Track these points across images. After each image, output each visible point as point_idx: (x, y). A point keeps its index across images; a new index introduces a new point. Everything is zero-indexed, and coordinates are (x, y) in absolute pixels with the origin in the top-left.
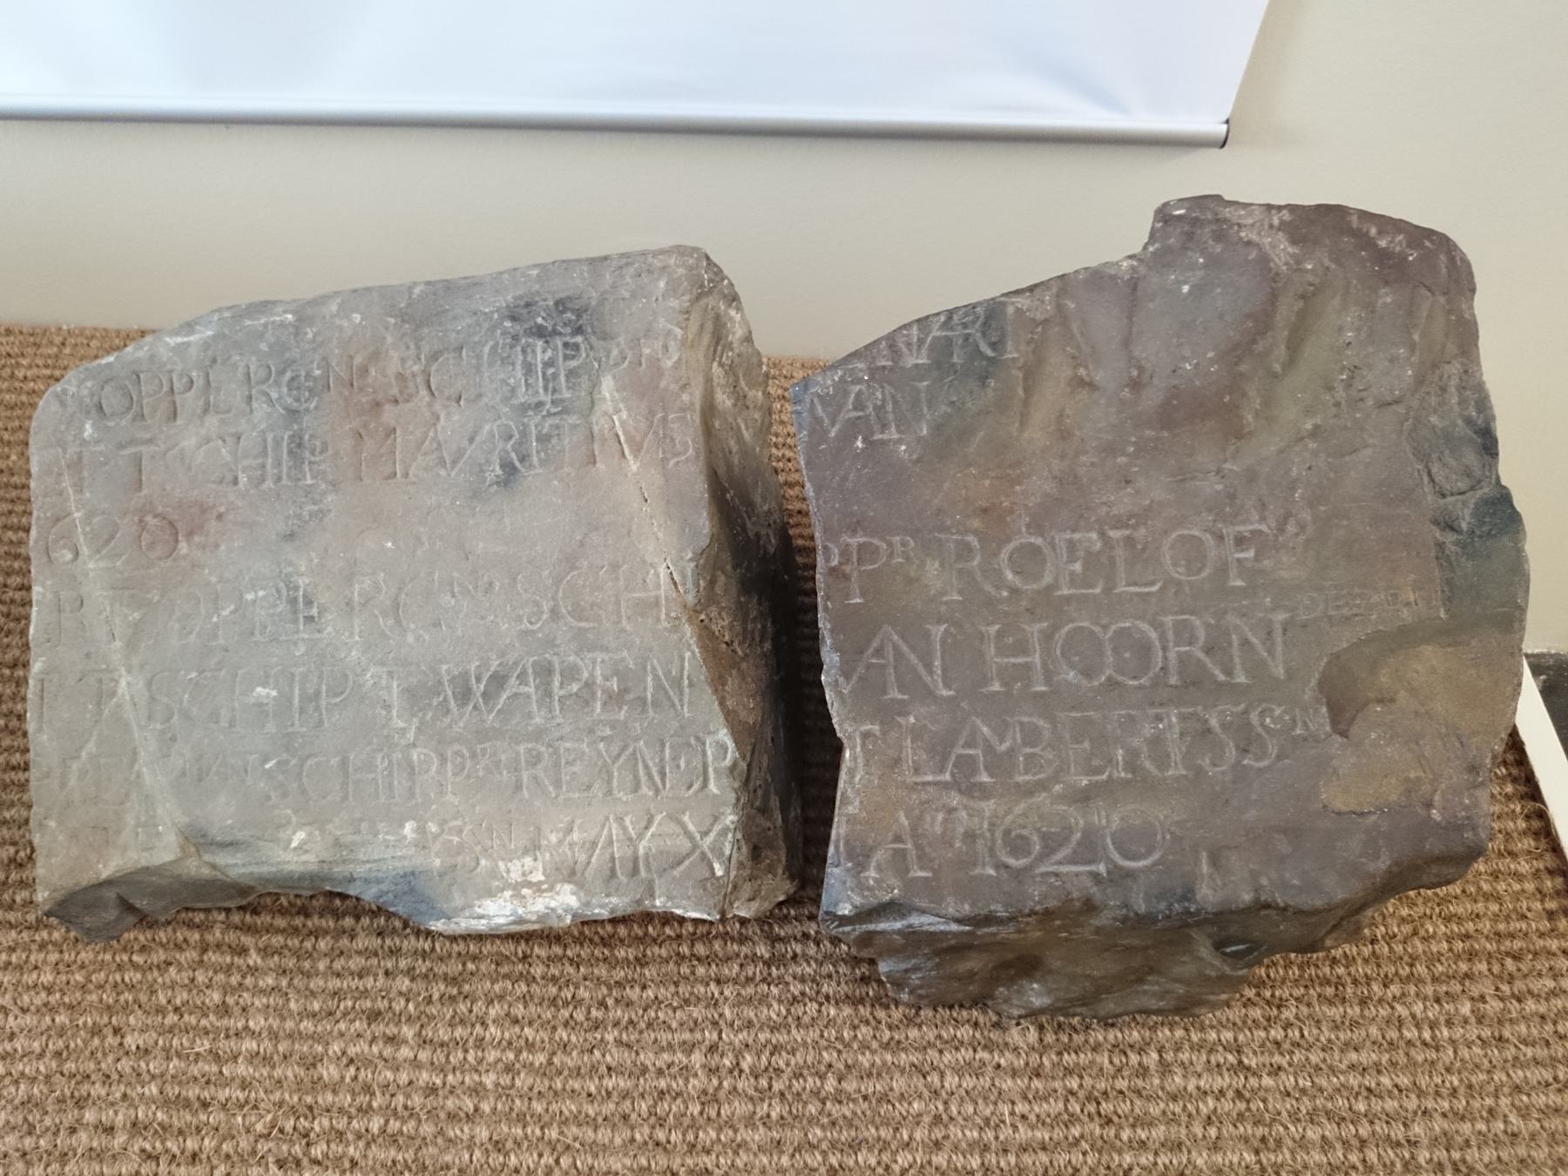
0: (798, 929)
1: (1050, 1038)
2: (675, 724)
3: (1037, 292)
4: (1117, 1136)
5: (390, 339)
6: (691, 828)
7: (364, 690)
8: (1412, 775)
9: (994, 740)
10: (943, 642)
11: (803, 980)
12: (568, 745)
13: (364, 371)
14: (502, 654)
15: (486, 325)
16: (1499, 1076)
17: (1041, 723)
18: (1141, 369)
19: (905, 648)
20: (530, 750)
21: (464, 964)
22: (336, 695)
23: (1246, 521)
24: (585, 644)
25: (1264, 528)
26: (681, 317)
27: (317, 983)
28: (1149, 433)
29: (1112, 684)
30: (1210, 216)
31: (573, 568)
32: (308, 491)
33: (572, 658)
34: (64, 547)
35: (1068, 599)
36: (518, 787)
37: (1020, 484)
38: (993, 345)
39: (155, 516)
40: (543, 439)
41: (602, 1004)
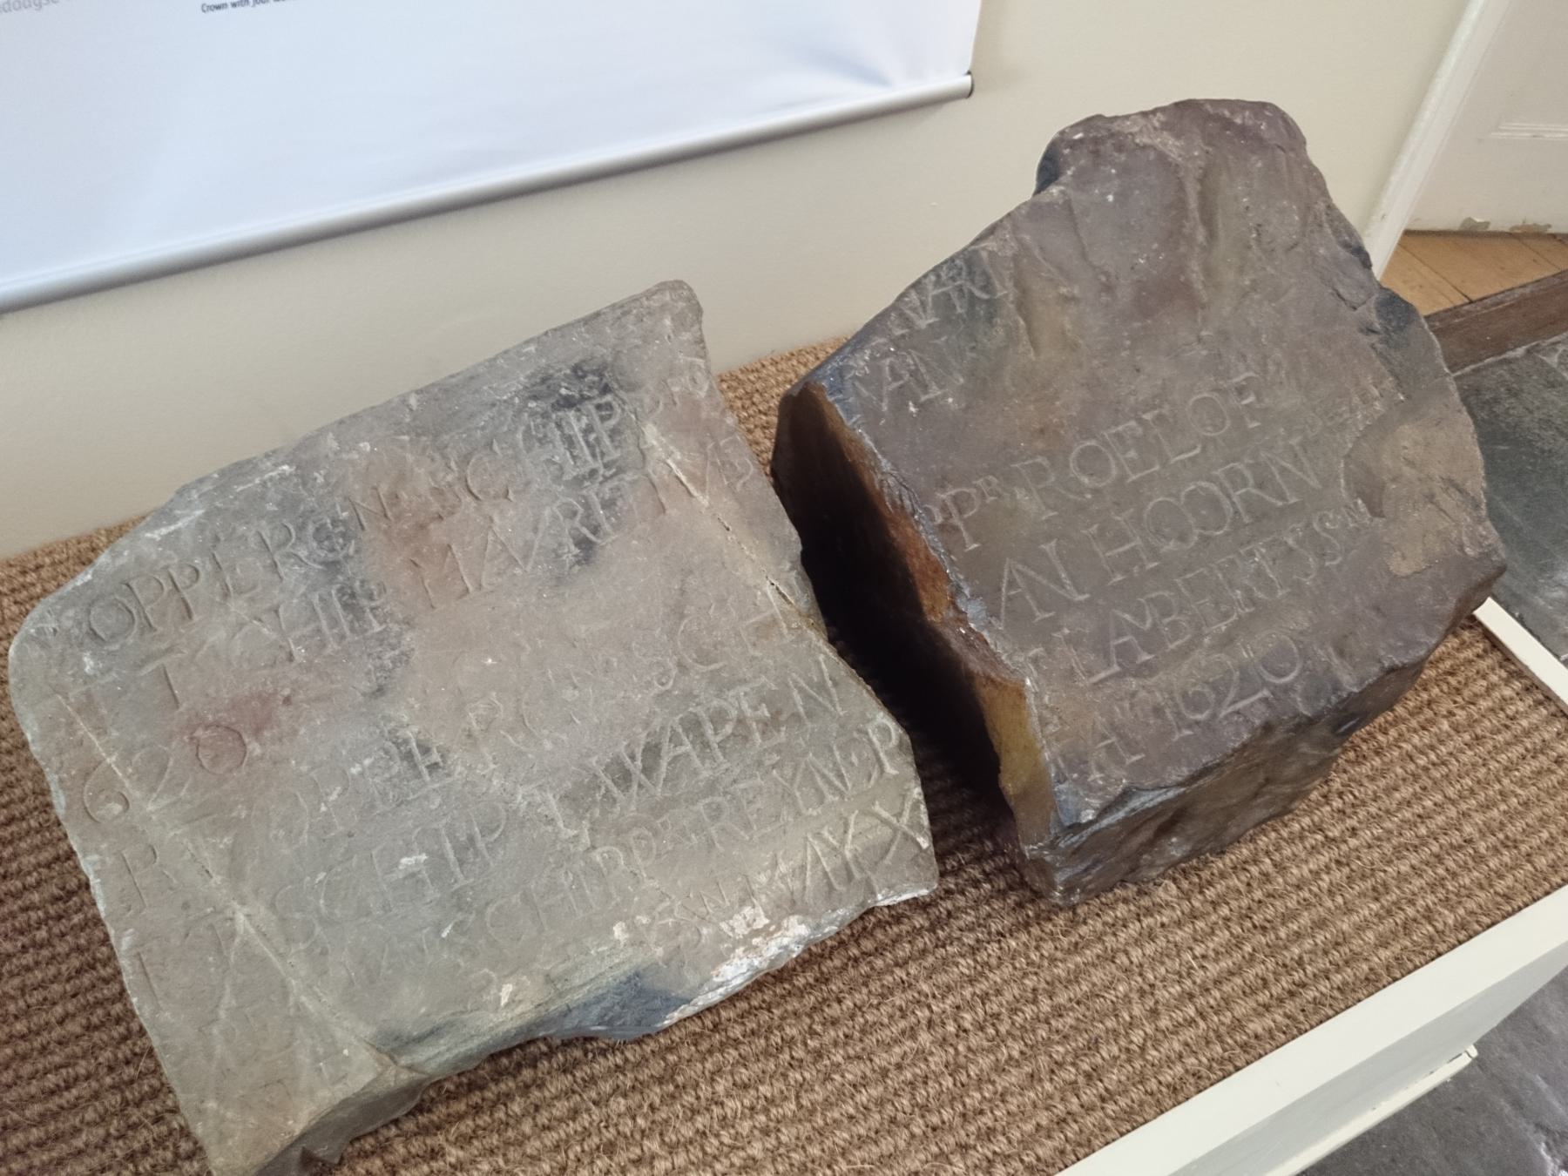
1: (1185, 885)
2: (835, 726)
3: (999, 233)
4: (1278, 938)
5: (410, 458)
6: (885, 814)
7: (520, 814)
11: (971, 930)
12: (742, 786)
14: (647, 724)
15: (510, 413)
16: (1493, 765)
17: (1166, 594)
18: (1106, 274)
20: (709, 805)
21: (664, 1059)
22: (493, 831)
23: (1238, 373)
24: (722, 686)
25: (1251, 374)
26: (698, 348)
27: (532, 1147)
28: (1137, 325)
29: (1205, 540)
30: (1104, 133)
31: (682, 616)
32: (381, 639)
33: (715, 703)
34: (108, 799)
36: (711, 845)
37: (1058, 399)
39: (207, 727)
40: (608, 504)
41: (813, 1033)
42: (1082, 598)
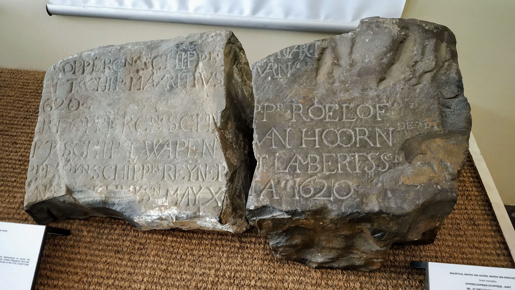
0: (249, 240)
5: (144, 53)
6: (213, 191)
8: (431, 175)
9: (302, 161)
10: (289, 132)
13: (136, 61)
14: (163, 138)
19: (278, 134)
25: (388, 104)
33: (183, 140)
35: (328, 122)
38: (310, 54)
40: (182, 79)
42: (288, 147)
